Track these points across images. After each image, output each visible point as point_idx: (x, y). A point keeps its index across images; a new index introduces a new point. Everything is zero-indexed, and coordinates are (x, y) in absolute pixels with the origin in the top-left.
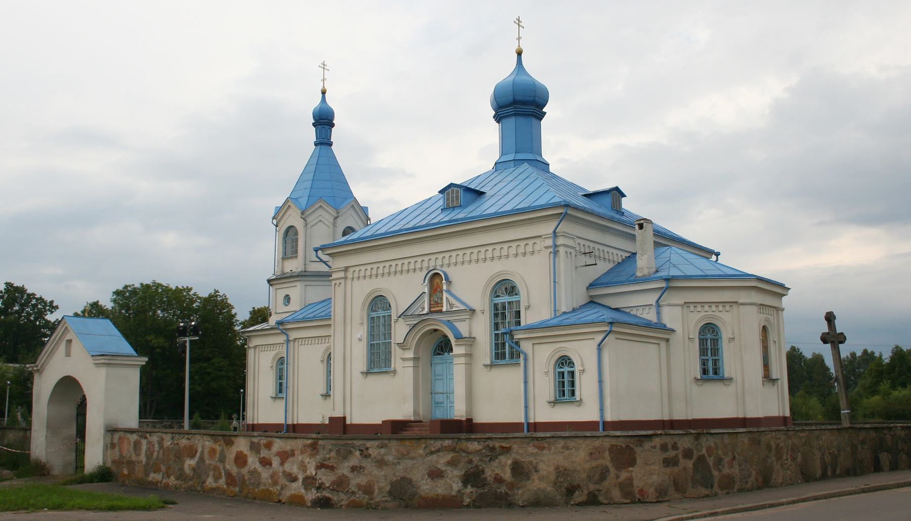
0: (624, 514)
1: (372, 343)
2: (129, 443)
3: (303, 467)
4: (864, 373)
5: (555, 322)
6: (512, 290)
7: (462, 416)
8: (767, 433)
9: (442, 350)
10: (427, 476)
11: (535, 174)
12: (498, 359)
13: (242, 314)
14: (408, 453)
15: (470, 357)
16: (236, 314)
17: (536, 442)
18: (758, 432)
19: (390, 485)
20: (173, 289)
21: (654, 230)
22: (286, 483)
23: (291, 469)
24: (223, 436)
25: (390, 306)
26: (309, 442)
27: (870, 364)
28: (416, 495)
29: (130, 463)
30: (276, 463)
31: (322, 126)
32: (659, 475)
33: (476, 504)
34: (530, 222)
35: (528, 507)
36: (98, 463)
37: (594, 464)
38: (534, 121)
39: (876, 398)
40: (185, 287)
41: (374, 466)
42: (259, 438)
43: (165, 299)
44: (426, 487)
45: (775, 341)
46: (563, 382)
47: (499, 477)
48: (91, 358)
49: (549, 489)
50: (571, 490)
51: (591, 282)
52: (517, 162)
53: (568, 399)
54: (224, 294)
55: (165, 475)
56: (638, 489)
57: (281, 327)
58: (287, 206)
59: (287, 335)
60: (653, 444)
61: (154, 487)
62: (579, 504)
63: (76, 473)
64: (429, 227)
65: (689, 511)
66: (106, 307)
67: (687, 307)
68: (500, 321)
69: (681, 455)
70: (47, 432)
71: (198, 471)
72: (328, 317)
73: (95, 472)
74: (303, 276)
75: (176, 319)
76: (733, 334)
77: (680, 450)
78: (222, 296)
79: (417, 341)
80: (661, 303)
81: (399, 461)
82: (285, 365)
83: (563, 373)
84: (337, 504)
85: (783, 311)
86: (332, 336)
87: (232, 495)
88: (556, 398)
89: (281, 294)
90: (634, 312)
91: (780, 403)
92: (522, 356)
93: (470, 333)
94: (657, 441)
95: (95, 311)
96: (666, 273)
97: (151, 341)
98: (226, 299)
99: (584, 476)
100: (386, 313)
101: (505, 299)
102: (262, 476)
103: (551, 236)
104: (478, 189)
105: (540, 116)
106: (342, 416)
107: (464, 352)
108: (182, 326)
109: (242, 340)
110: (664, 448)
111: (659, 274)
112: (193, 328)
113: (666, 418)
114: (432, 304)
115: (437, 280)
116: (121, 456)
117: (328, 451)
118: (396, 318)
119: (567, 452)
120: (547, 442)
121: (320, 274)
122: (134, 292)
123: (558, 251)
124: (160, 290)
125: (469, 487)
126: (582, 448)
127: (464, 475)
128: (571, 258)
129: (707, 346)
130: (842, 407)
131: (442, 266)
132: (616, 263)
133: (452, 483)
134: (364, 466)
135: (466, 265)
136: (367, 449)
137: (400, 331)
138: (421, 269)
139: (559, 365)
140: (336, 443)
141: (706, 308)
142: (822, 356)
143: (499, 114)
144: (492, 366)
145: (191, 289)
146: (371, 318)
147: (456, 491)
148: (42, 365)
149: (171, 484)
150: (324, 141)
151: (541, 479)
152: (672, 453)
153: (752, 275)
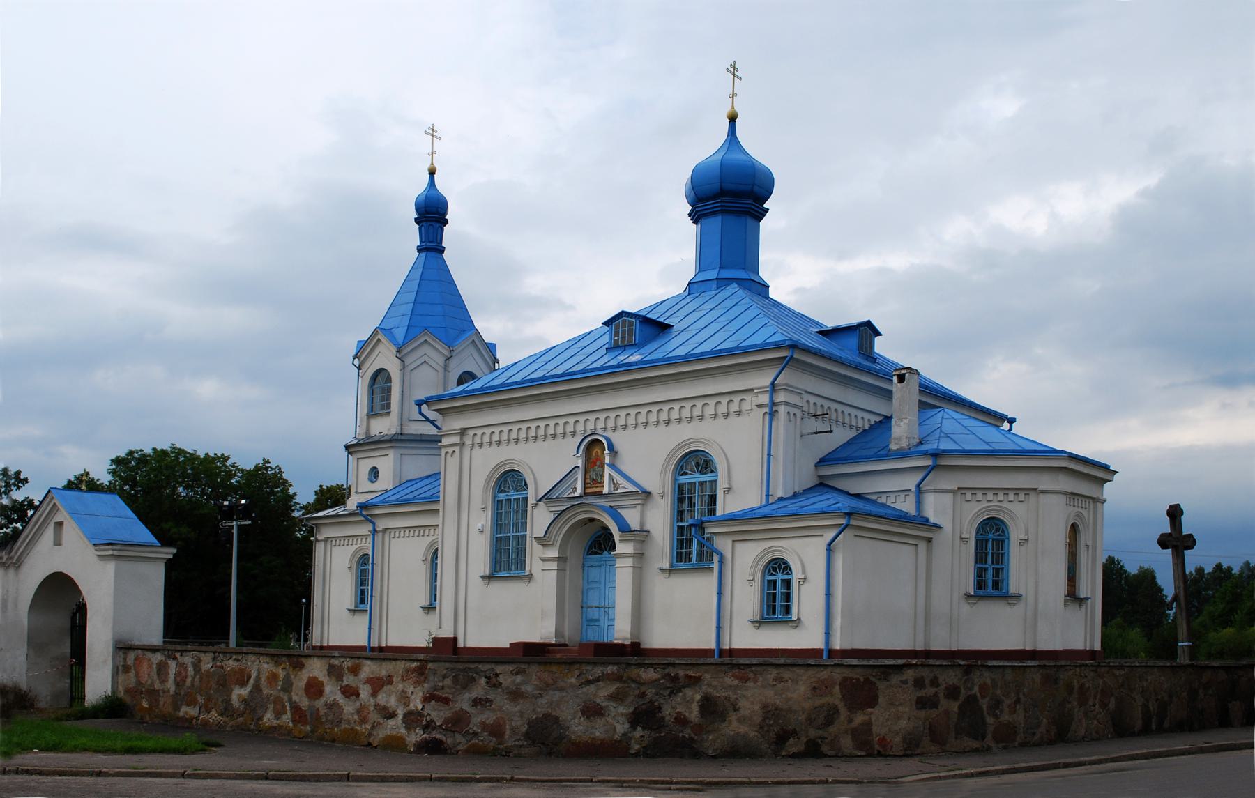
0: (857, 770)
1: (498, 536)
2: (150, 666)
3: (404, 698)
4: (1214, 597)
5: (766, 510)
6: (706, 465)
7: (625, 639)
8: (1068, 668)
9: (600, 548)
10: (580, 714)
11: (747, 300)
12: (681, 562)
13: (304, 494)
14: (555, 682)
15: (641, 558)
16: (295, 494)
17: (736, 671)
18: (1054, 666)
19: (528, 724)
20: (202, 457)
21: (921, 385)
22: (379, 720)
23: (387, 702)
24: (289, 656)
25: (526, 485)
26: (415, 665)
27: (1224, 584)
28: (564, 738)
29: (153, 693)
30: (366, 693)
31: (429, 223)
32: (909, 719)
33: (649, 752)
34: (748, 368)
35: (721, 758)
36: (105, 692)
37: (818, 702)
38: (750, 221)
39: (1230, 631)
40: (219, 455)
41: (506, 699)
42: (342, 660)
43: (189, 471)
44: (578, 728)
45: (1088, 546)
46: (774, 595)
47: (682, 717)
48: (92, 548)
49: (752, 734)
50: (782, 738)
51: (822, 456)
52: (722, 282)
53: (780, 618)
54: (278, 466)
55: (203, 709)
56: (878, 738)
57: (364, 513)
58: (376, 340)
59: (374, 524)
60: (904, 678)
61: (186, 725)
62: (794, 756)
63: (71, 706)
64: (587, 374)
65: (950, 768)
66: (100, 482)
67: (962, 494)
68: (686, 509)
69: (942, 694)
70: (28, 649)
71: (251, 704)
72: (435, 499)
73: (101, 705)
74: (398, 440)
75: (205, 499)
76: (1027, 534)
77: (942, 687)
78: (275, 468)
79: (563, 538)
80: (924, 487)
81: (541, 692)
82: (370, 565)
83: (775, 582)
84: (451, 749)
85: (1103, 503)
86: (440, 527)
87: (301, 736)
88: (763, 617)
89: (366, 465)
90: (883, 500)
91: (1088, 635)
92: (716, 559)
93: (642, 524)
94: (910, 674)
95: (82, 484)
96: (935, 446)
97: (169, 530)
98: (281, 473)
99: (802, 717)
100: (520, 495)
101: (696, 477)
102: (345, 711)
103: (768, 389)
104: (661, 320)
105: (761, 213)
106: (452, 636)
107: (633, 551)
108: (226, 506)
109: (304, 531)
110: (919, 683)
111: (923, 447)
112: (243, 509)
113: (920, 647)
114: (588, 484)
115: (597, 450)
116: (139, 683)
117: (441, 678)
118: (535, 502)
119: (780, 686)
120: (752, 671)
121: (423, 438)
122: (144, 460)
123: (776, 411)
124: (183, 459)
125: (639, 729)
126: (801, 680)
127: (633, 713)
128: (796, 423)
129: (986, 549)
130: (1180, 637)
131: (605, 429)
132: (861, 430)
133: (616, 723)
134: (492, 698)
135: (641, 429)
136: (497, 675)
137: (540, 520)
138: (574, 434)
139: (769, 571)
140: (452, 667)
141: (990, 496)
142: (1153, 571)
143: (696, 210)
144: (671, 570)
145: (228, 457)
146: (498, 501)
147: (620, 735)
148: (18, 557)
149: (211, 721)
150: (431, 245)
151: (741, 720)
152: (930, 691)
153: (1062, 451)
